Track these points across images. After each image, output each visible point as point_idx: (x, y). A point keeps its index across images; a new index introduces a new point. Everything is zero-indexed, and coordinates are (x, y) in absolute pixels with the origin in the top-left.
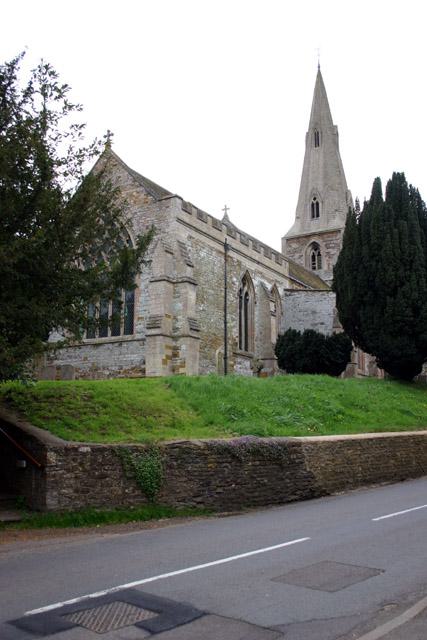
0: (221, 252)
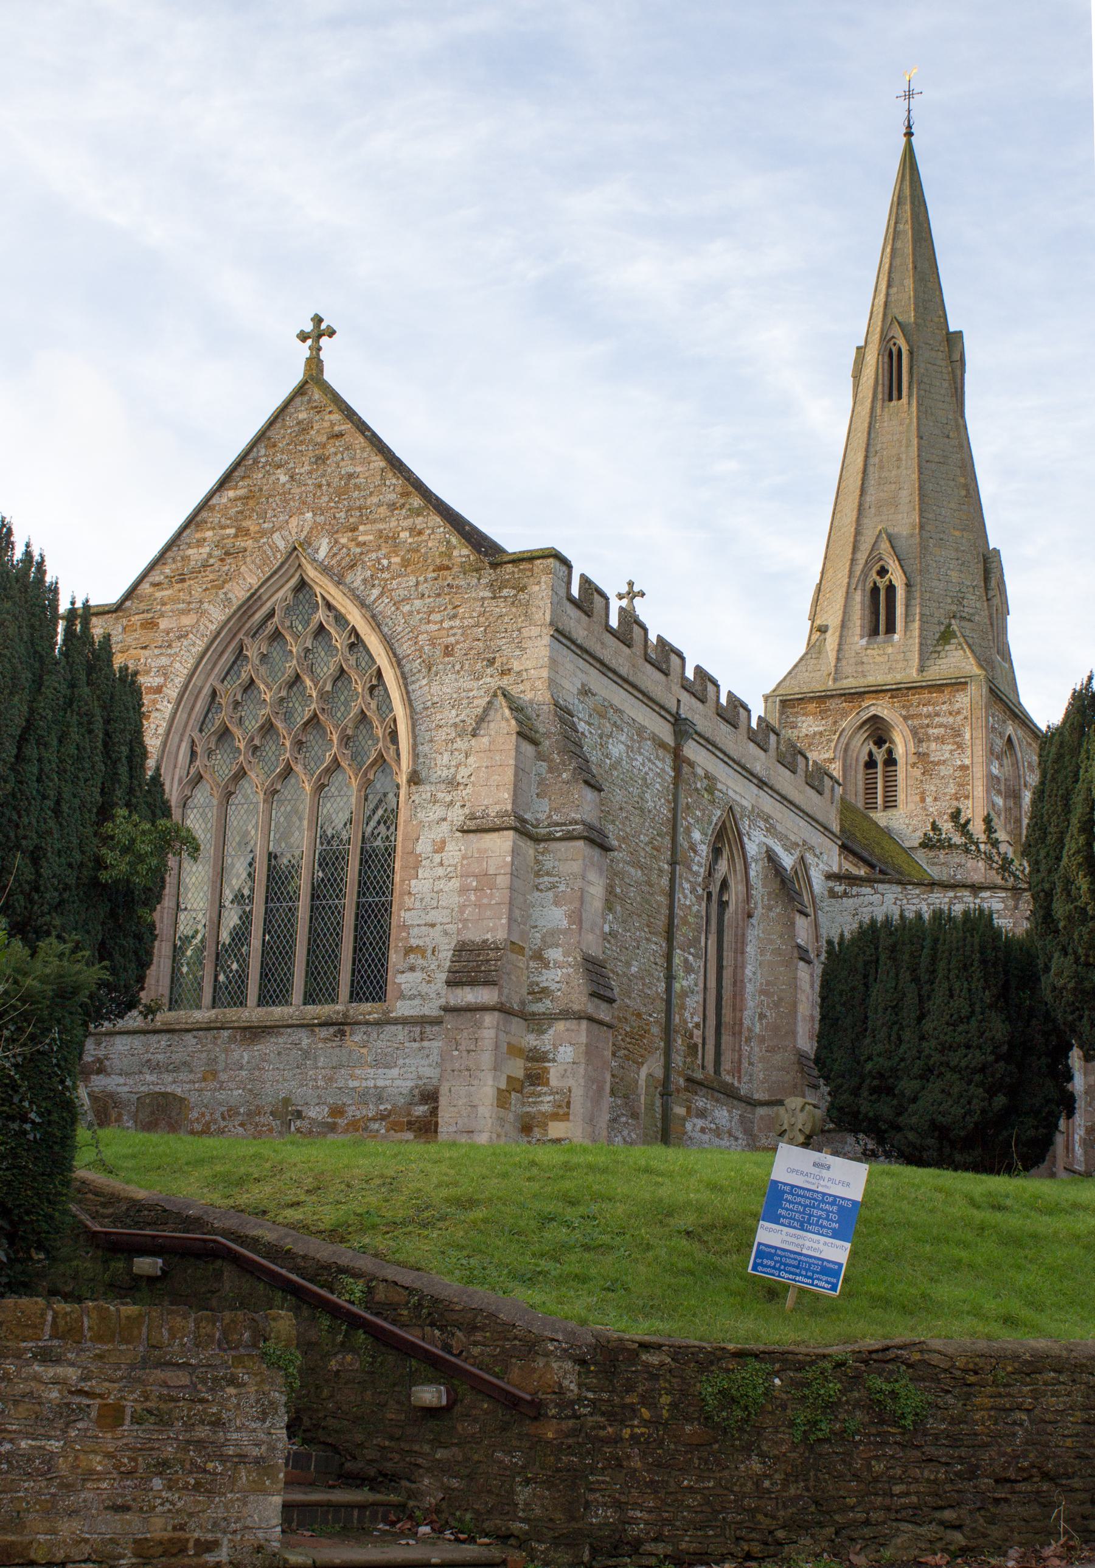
0: (662, 745)
